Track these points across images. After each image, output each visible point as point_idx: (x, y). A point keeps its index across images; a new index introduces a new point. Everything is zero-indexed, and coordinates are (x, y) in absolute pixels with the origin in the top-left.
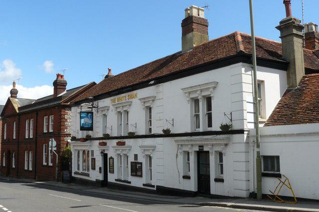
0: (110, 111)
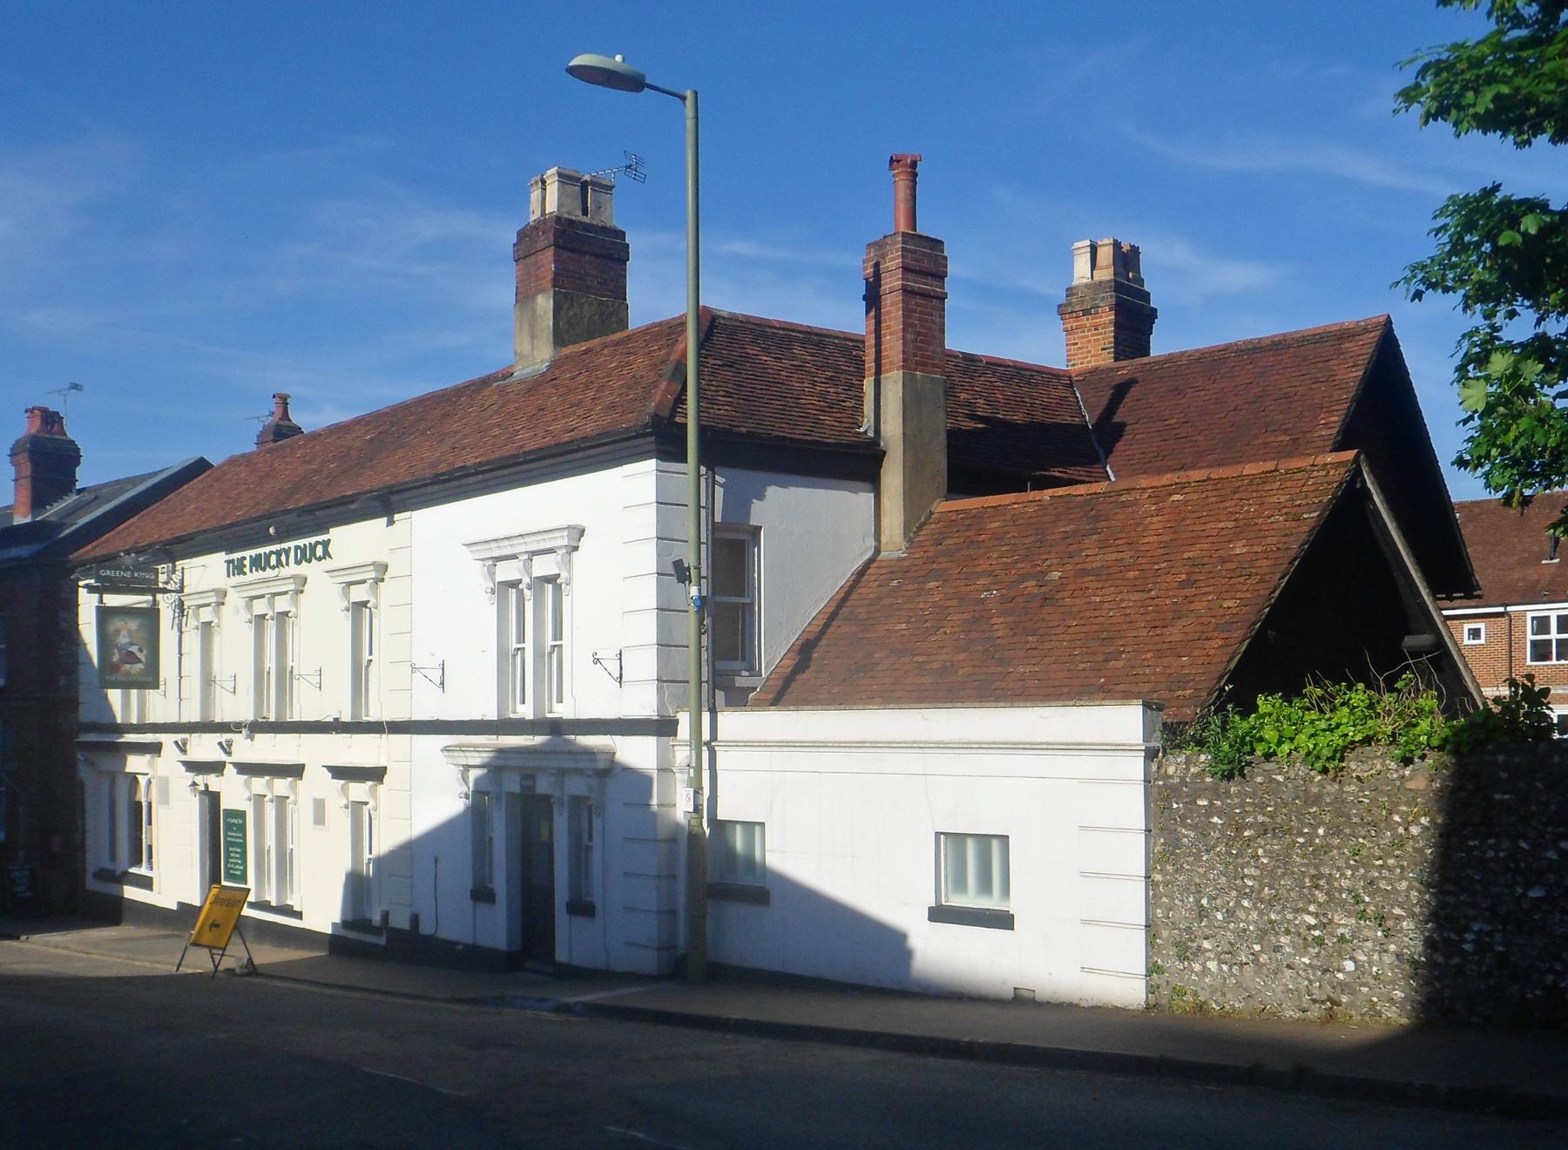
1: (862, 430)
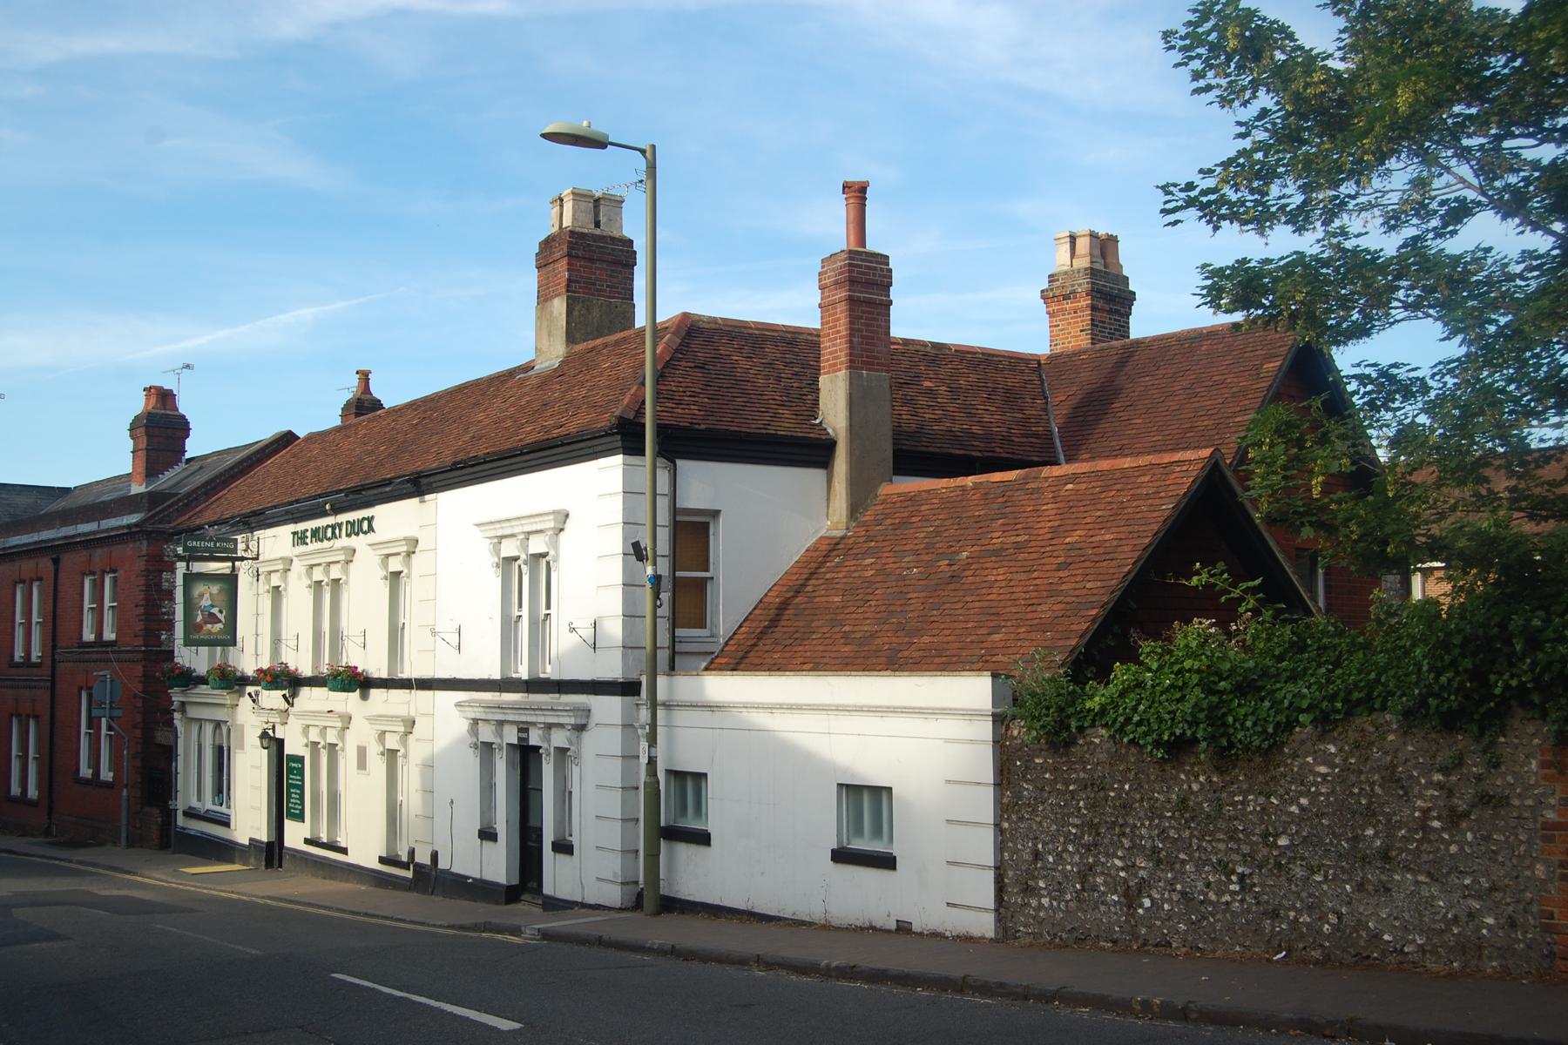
0: (292, 576)
1: (817, 421)
